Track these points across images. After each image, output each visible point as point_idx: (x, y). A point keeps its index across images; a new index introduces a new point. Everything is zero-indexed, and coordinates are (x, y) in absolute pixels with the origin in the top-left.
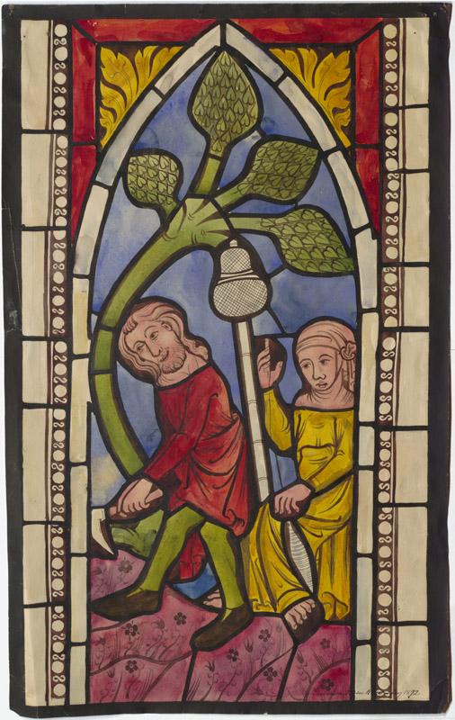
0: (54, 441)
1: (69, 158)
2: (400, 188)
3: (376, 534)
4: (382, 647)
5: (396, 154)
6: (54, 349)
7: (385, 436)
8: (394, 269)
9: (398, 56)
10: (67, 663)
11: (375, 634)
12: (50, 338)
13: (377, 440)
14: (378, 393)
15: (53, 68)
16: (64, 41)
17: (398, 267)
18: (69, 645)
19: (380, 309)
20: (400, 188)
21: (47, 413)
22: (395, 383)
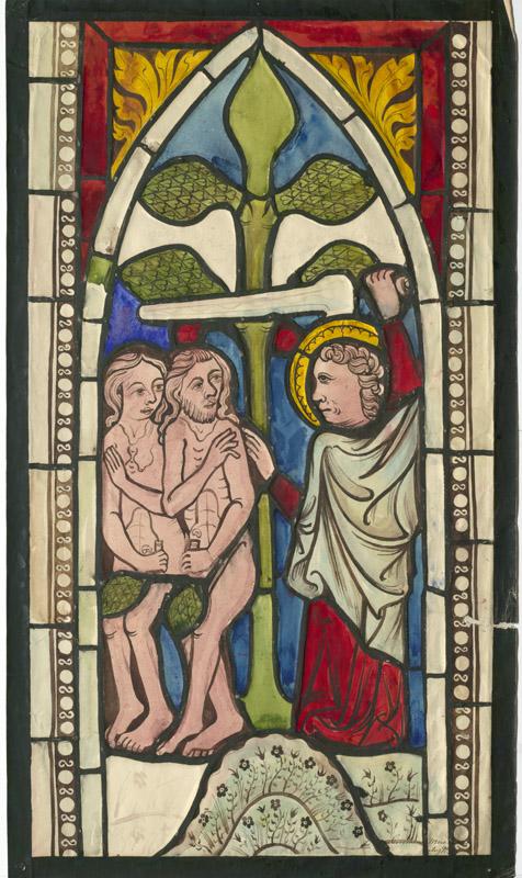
0: (58, 390)
1: (78, 176)
2: (468, 504)
3: (447, 424)
4: (459, 732)
5: (468, 845)
6: (58, 649)
7: (455, 312)
8: (468, 711)
9: (463, 338)
10: (77, 798)
11: (74, 655)
12: (58, 300)
13: (446, 320)
14: (446, 371)
15: (60, 844)
16: (68, 347)
17: (471, 708)
18: (77, 380)
19: (449, 815)
20: (468, 504)
21: (50, 475)
22: (473, 819)
